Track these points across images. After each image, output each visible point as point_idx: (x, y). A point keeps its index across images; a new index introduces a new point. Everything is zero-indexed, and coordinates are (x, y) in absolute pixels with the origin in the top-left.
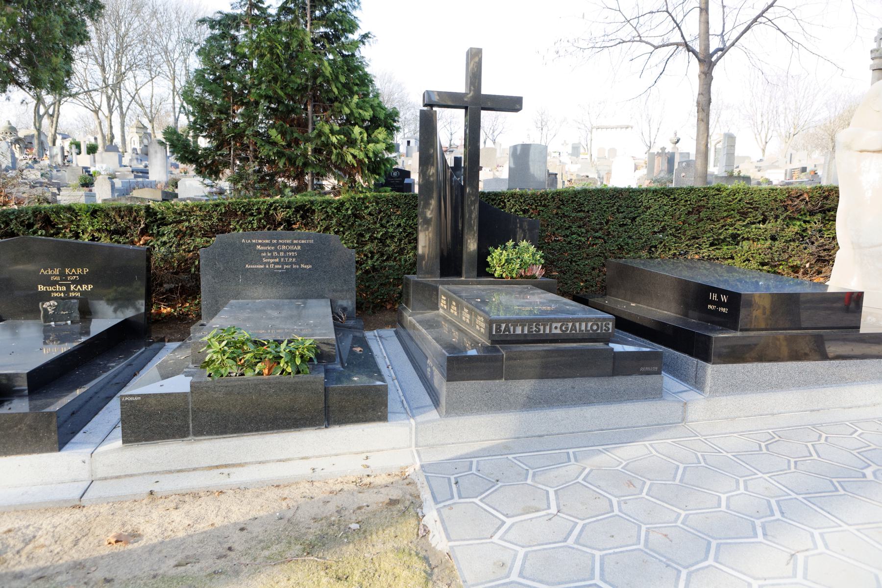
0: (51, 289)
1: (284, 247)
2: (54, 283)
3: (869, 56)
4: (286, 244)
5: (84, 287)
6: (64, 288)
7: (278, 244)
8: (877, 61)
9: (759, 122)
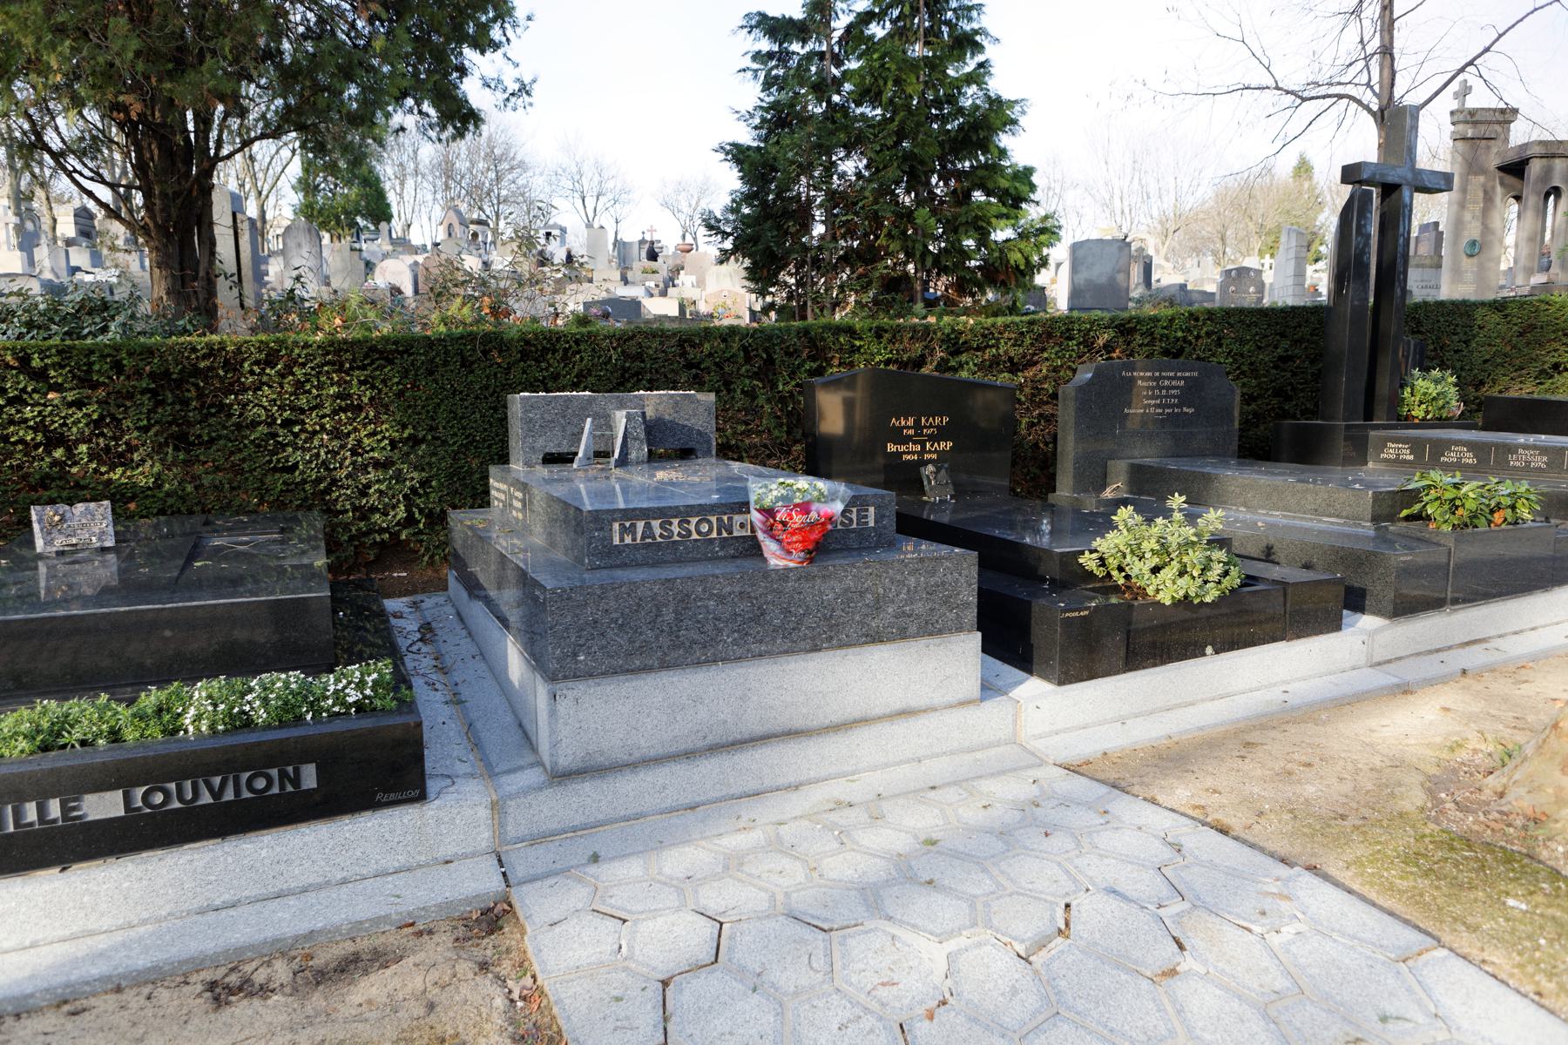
0: (903, 448)
1: (1167, 383)
2: (906, 440)
3: (1448, 119)
4: (1169, 378)
5: (942, 444)
6: (919, 448)
7: (1161, 378)
8: (1460, 127)
9: (1118, 212)
